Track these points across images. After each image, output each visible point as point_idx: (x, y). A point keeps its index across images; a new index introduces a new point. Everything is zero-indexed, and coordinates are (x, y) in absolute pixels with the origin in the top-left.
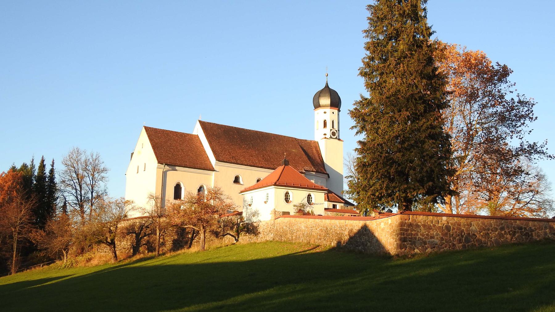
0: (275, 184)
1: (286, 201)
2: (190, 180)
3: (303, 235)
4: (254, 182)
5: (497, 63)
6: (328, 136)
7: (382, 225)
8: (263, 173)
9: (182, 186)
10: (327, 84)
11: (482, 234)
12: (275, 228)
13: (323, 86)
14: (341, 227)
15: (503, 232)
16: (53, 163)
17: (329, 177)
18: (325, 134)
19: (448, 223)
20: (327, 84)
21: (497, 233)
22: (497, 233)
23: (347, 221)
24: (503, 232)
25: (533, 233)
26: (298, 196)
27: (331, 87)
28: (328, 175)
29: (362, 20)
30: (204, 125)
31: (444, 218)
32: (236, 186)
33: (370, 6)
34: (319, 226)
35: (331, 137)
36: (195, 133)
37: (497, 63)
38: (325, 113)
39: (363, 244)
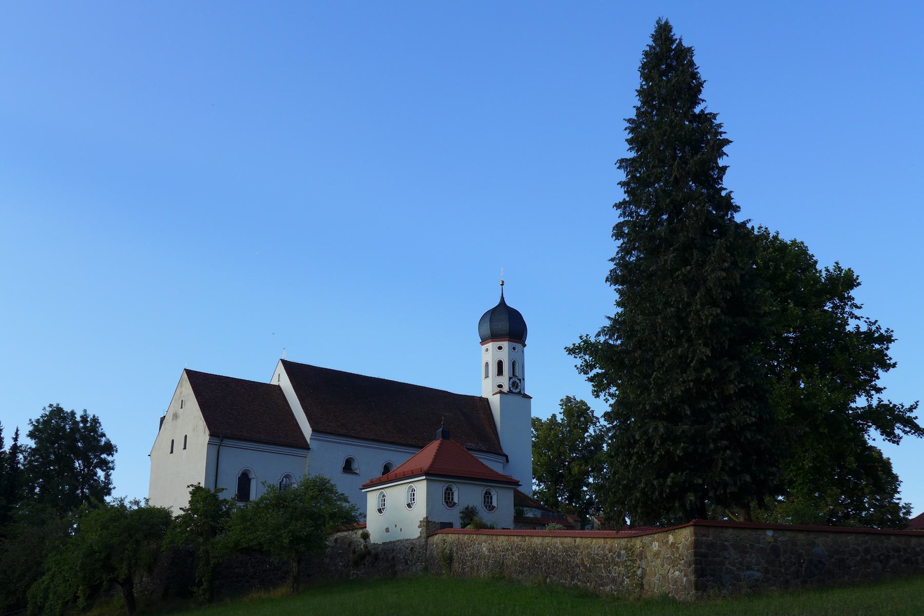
0: (426, 474)
1: (447, 503)
2: (269, 469)
3: (487, 564)
4: (378, 474)
5: (837, 263)
6: (506, 389)
7: (655, 546)
8: (399, 458)
9: (252, 476)
10: (502, 298)
11: (833, 560)
12: (428, 552)
13: (496, 303)
14: (566, 550)
15: (869, 557)
16: (17, 434)
17: (508, 461)
18: (500, 386)
19: (776, 541)
20: (502, 298)
21: (858, 558)
22: (858, 558)
23: (578, 540)
24: (869, 557)
25: (919, 558)
26: (468, 495)
27: (509, 303)
28: (507, 457)
29: (611, 188)
30: (291, 368)
31: (770, 533)
32: (349, 477)
33: (622, 161)
34: (519, 548)
35: (510, 392)
36: (275, 382)
37: (837, 263)
38: (500, 348)
39: (614, 581)
